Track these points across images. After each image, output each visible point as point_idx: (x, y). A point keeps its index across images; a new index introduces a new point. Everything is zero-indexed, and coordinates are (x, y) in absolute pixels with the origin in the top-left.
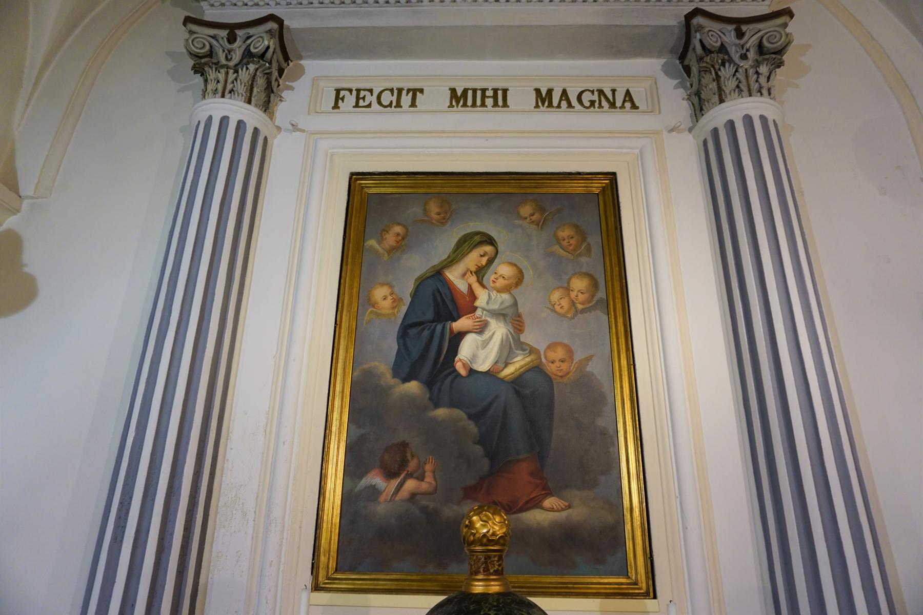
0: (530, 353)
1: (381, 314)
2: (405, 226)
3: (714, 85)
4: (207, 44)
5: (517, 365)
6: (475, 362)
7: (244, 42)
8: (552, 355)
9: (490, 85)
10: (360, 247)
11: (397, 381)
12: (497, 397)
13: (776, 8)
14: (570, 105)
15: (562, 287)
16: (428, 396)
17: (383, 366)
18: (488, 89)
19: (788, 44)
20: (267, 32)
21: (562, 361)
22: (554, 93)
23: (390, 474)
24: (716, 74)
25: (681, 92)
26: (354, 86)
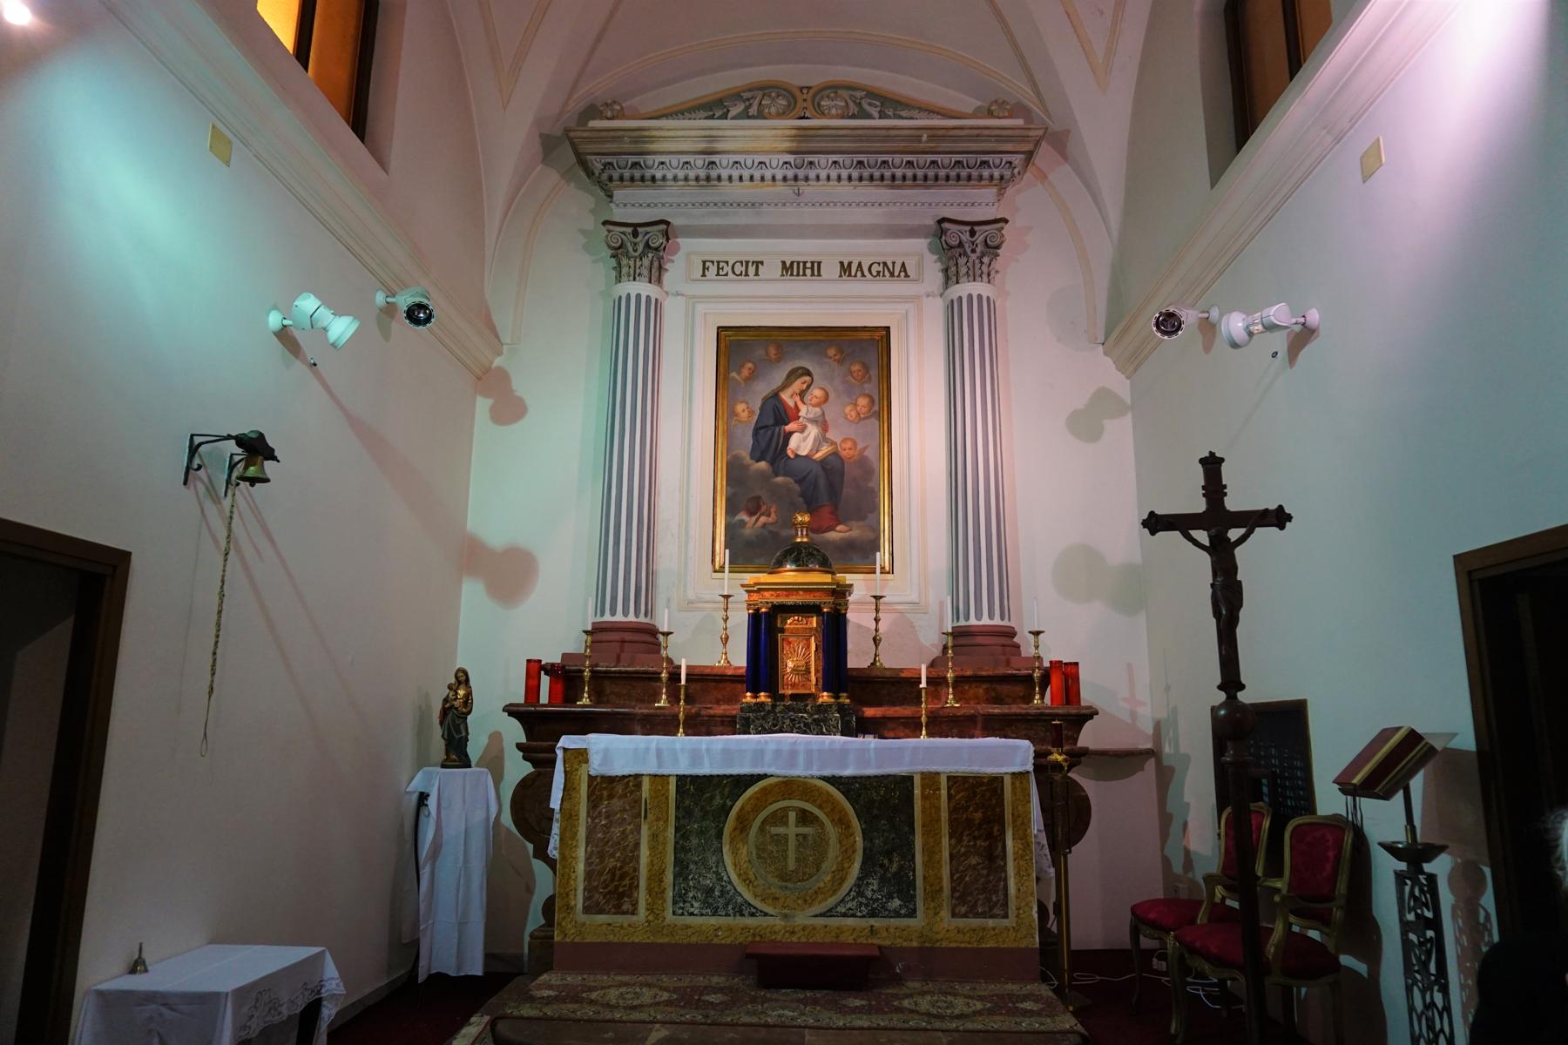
3: (954, 269)
5: (823, 452)
8: (844, 446)
9: (809, 259)
10: (726, 378)
11: (753, 461)
12: (811, 471)
14: (863, 275)
16: (771, 470)
17: (745, 453)
19: (1002, 242)
20: (659, 231)
21: (850, 449)
23: (751, 514)
25: (939, 266)
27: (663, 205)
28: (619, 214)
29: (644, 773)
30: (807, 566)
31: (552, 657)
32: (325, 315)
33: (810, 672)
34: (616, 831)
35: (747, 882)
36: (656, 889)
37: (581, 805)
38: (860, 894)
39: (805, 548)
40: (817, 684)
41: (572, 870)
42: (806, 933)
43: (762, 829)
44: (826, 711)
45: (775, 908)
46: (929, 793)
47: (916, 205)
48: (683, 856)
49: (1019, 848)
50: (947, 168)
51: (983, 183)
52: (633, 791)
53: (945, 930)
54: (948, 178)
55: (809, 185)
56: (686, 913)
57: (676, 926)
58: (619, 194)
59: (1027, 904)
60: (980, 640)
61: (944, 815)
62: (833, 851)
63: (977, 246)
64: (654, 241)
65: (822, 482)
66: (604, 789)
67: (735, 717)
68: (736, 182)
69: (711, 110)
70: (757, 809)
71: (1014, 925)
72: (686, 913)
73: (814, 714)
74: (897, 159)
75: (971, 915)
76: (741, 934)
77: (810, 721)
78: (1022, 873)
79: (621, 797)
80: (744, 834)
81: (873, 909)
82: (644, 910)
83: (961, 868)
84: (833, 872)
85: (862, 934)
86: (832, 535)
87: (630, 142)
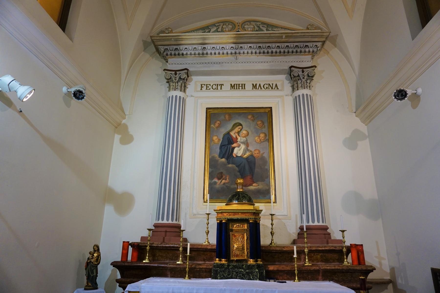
0: (250, 152)
1: (215, 143)
2: (220, 122)
3: (296, 85)
4: (170, 76)
5: (247, 155)
6: (238, 154)
7: (179, 75)
8: (255, 152)
9: (241, 83)
10: (209, 127)
11: (220, 158)
14: (261, 88)
15: (258, 136)
16: (227, 162)
17: (216, 155)
18: (240, 84)
19: (314, 75)
21: (258, 153)
22: (257, 85)
23: (219, 179)
24: (297, 82)
25: (290, 85)
26: (206, 84)
28: (169, 67)
30: (242, 202)
31: (137, 239)
32: (15, 85)
33: (244, 249)
40: (247, 255)
44: (252, 268)
47: (281, 62)
50: (292, 48)
51: (306, 53)
54: (293, 52)
55: (240, 56)
58: (170, 60)
60: (314, 232)
63: (305, 76)
65: (247, 167)
67: (211, 269)
69: (204, 30)
74: (274, 45)
77: (245, 273)
86: (251, 188)
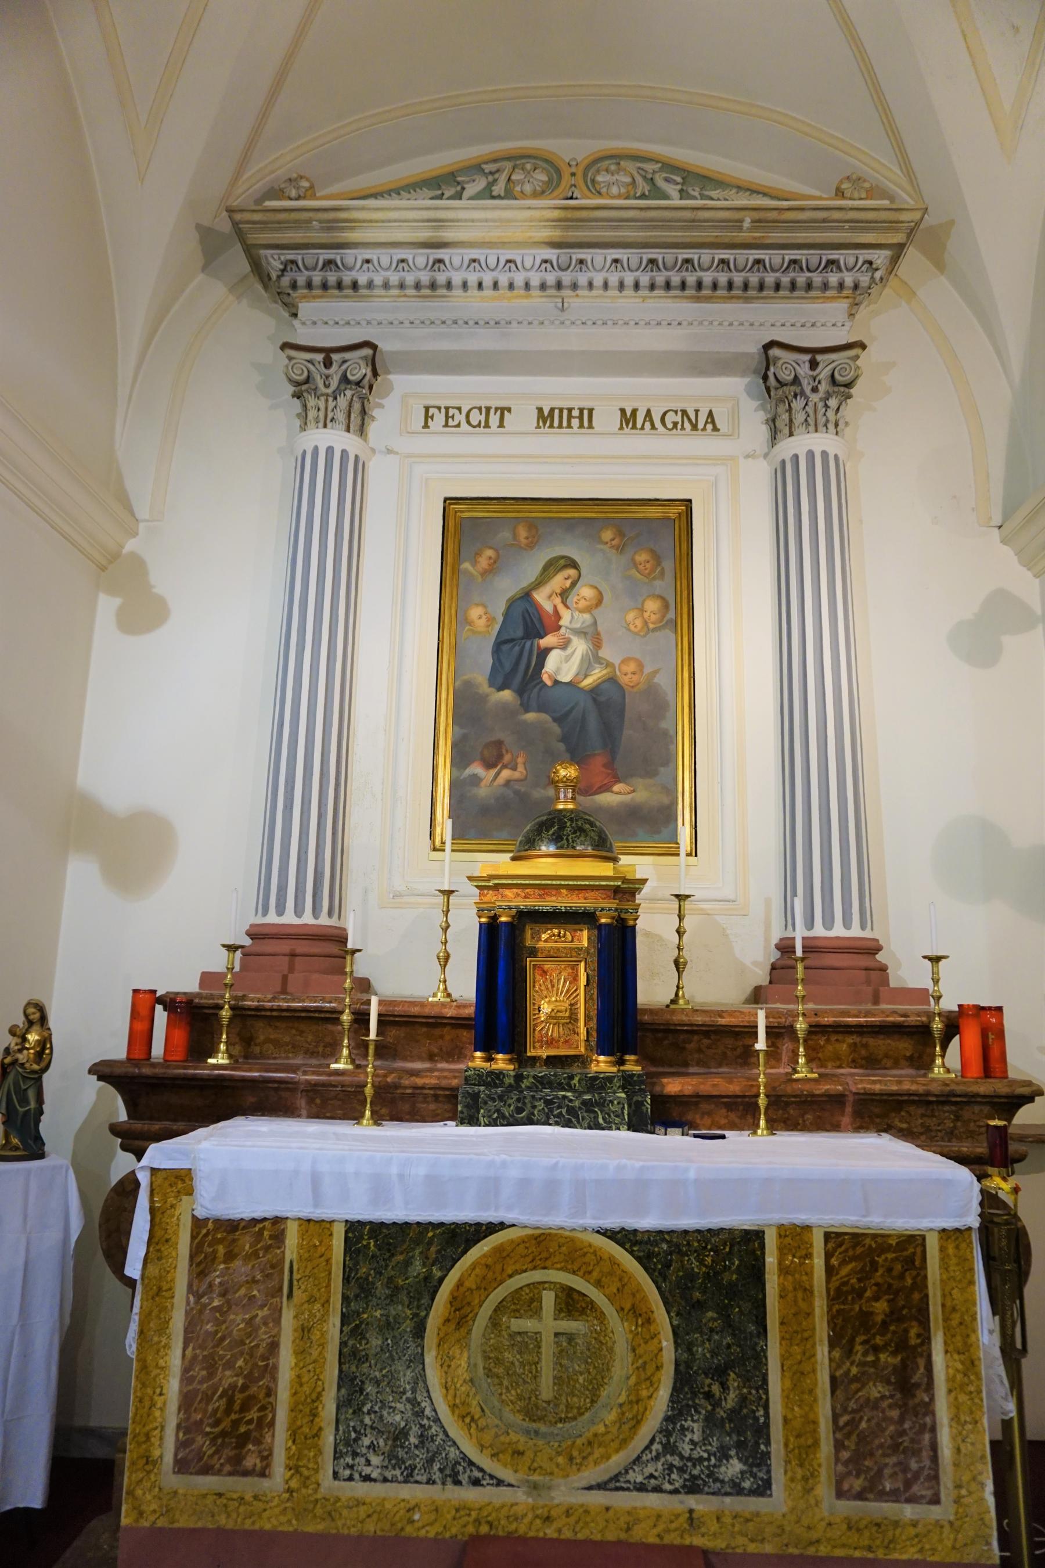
2: (496, 550)
3: (785, 417)
5: (595, 677)
8: (625, 668)
9: (576, 404)
10: (456, 570)
11: (493, 690)
12: (577, 704)
13: (852, 340)
14: (653, 427)
17: (480, 676)
19: (857, 377)
20: (362, 358)
21: (634, 673)
23: (489, 765)
25: (762, 416)
26: (443, 404)
27: (369, 323)
28: (303, 335)
29: (289, 1215)
30: (574, 848)
33: (577, 1020)
34: (238, 1319)
35: (468, 1420)
36: (305, 1429)
37: (179, 1269)
38: (670, 1448)
39: (571, 820)
40: (587, 1040)
41: (158, 1391)
42: (572, 1520)
43: (494, 1323)
45: (516, 1471)
46: (792, 1262)
48: (354, 1368)
49: (957, 1370)
51: (829, 293)
52: (270, 1246)
53: (823, 1524)
54: (778, 287)
55: (577, 296)
56: (356, 1476)
57: (338, 1500)
58: (305, 308)
59: (974, 1479)
61: (820, 1305)
62: (622, 1365)
63: (819, 382)
64: (355, 372)
65: (593, 723)
66: (221, 1241)
68: (473, 292)
69: (440, 188)
70: (486, 1286)
71: (952, 1518)
72: (356, 1476)
73: (584, 1093)
74: (706, 256)
75: (871, 1496)
76: (454, 1519)
77: (577, 1104)
78: (962, 1418)
79: (247, 1258)
80: (463, 1331)
81: (694, 1478)
82: (282, 1470)
83: (852, 1405)
84: (621, 1405)
85: (673, 1526)
86: (606, 799)
87: (322, 228)
